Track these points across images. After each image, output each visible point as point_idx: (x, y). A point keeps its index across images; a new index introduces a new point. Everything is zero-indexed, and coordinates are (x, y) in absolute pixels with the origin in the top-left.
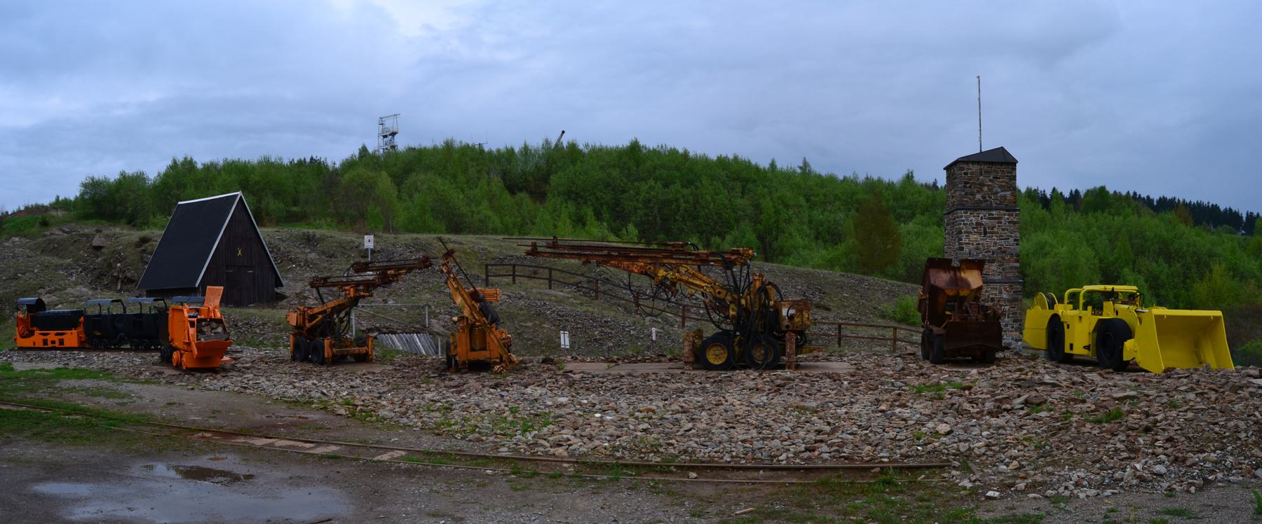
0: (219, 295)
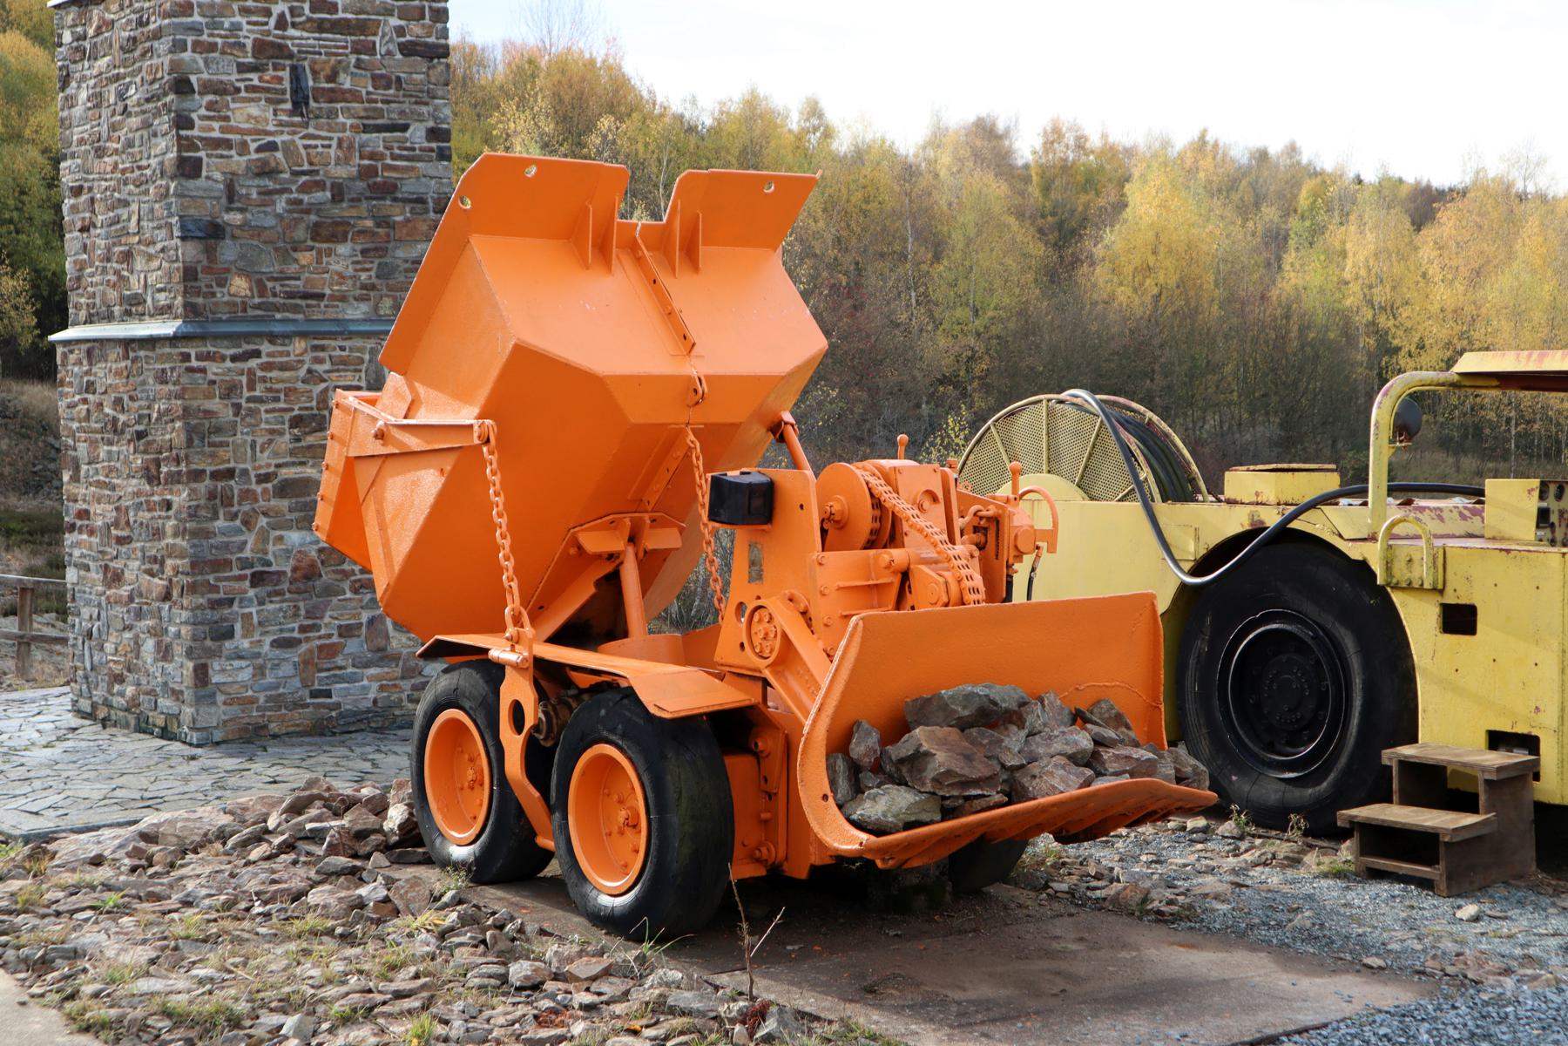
0: (477, 783)
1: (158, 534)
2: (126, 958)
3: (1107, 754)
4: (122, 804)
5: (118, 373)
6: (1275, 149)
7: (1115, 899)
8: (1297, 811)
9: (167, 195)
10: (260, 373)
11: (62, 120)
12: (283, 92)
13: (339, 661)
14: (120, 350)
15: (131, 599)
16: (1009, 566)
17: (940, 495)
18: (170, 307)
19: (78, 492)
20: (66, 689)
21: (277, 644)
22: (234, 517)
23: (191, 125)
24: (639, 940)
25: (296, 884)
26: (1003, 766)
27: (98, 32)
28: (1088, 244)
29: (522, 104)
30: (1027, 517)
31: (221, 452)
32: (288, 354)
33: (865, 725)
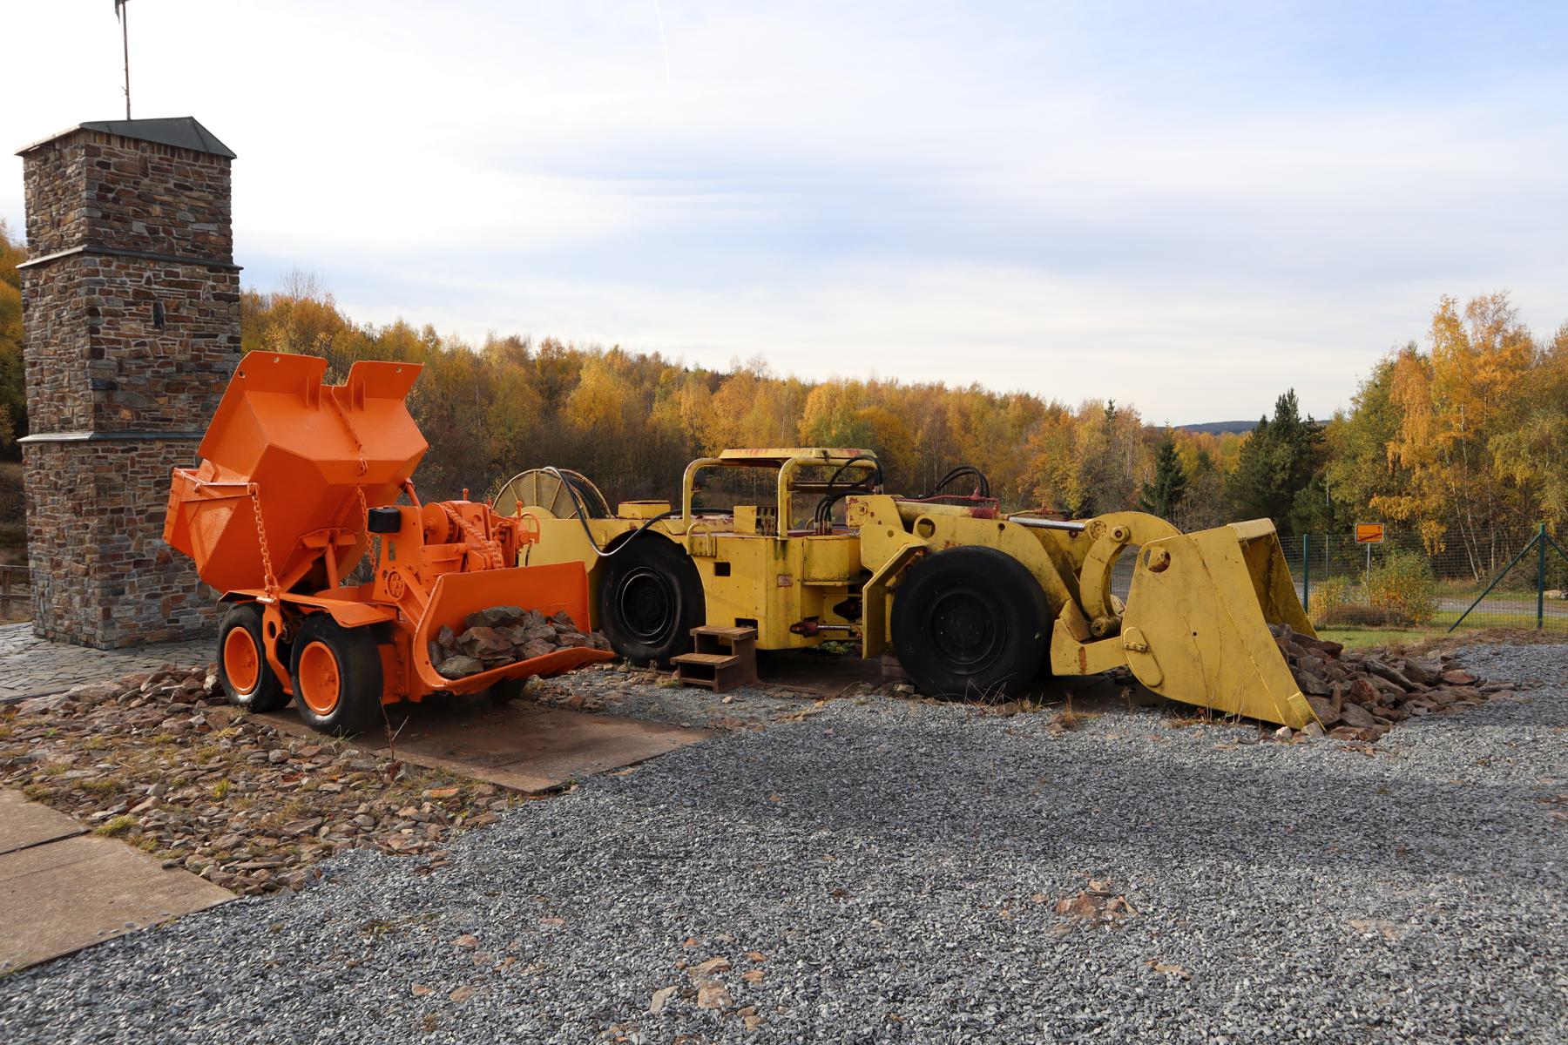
1: (81, 542)
2: (60, 761)
3: (562, 637)
4: (63, 682)
5: (57, 459)
6: (649, 355)
7: (569, 704)
8: (654, 658)
9: (84, 367)
10: (137, 459)
11: (25, 327)
12: (150, 316)
13: (183, 604)
14: (59, 447)
15: (66, 575)
16: (517, 550)
17: (482, 517)
18: (86, 425)
19: (35, 521)
20: (30, 623)
21: (149, 596)
22: (124, 532)
23: (98, 332)
24: (337, 736)
25: (156, 718)
26: (513, 644)
27: (46, 282)
28: (563, 397)
29: (281, 325)
30: (524, 526)
31: (116, 499)
32: (153, 449)
33: (446, 628)
